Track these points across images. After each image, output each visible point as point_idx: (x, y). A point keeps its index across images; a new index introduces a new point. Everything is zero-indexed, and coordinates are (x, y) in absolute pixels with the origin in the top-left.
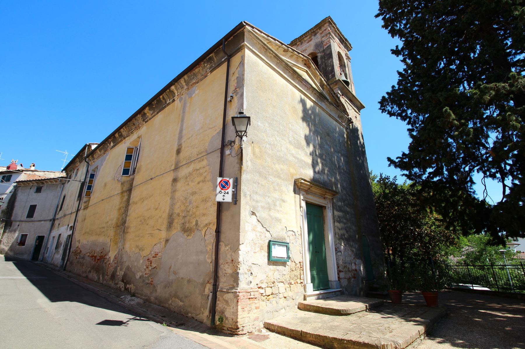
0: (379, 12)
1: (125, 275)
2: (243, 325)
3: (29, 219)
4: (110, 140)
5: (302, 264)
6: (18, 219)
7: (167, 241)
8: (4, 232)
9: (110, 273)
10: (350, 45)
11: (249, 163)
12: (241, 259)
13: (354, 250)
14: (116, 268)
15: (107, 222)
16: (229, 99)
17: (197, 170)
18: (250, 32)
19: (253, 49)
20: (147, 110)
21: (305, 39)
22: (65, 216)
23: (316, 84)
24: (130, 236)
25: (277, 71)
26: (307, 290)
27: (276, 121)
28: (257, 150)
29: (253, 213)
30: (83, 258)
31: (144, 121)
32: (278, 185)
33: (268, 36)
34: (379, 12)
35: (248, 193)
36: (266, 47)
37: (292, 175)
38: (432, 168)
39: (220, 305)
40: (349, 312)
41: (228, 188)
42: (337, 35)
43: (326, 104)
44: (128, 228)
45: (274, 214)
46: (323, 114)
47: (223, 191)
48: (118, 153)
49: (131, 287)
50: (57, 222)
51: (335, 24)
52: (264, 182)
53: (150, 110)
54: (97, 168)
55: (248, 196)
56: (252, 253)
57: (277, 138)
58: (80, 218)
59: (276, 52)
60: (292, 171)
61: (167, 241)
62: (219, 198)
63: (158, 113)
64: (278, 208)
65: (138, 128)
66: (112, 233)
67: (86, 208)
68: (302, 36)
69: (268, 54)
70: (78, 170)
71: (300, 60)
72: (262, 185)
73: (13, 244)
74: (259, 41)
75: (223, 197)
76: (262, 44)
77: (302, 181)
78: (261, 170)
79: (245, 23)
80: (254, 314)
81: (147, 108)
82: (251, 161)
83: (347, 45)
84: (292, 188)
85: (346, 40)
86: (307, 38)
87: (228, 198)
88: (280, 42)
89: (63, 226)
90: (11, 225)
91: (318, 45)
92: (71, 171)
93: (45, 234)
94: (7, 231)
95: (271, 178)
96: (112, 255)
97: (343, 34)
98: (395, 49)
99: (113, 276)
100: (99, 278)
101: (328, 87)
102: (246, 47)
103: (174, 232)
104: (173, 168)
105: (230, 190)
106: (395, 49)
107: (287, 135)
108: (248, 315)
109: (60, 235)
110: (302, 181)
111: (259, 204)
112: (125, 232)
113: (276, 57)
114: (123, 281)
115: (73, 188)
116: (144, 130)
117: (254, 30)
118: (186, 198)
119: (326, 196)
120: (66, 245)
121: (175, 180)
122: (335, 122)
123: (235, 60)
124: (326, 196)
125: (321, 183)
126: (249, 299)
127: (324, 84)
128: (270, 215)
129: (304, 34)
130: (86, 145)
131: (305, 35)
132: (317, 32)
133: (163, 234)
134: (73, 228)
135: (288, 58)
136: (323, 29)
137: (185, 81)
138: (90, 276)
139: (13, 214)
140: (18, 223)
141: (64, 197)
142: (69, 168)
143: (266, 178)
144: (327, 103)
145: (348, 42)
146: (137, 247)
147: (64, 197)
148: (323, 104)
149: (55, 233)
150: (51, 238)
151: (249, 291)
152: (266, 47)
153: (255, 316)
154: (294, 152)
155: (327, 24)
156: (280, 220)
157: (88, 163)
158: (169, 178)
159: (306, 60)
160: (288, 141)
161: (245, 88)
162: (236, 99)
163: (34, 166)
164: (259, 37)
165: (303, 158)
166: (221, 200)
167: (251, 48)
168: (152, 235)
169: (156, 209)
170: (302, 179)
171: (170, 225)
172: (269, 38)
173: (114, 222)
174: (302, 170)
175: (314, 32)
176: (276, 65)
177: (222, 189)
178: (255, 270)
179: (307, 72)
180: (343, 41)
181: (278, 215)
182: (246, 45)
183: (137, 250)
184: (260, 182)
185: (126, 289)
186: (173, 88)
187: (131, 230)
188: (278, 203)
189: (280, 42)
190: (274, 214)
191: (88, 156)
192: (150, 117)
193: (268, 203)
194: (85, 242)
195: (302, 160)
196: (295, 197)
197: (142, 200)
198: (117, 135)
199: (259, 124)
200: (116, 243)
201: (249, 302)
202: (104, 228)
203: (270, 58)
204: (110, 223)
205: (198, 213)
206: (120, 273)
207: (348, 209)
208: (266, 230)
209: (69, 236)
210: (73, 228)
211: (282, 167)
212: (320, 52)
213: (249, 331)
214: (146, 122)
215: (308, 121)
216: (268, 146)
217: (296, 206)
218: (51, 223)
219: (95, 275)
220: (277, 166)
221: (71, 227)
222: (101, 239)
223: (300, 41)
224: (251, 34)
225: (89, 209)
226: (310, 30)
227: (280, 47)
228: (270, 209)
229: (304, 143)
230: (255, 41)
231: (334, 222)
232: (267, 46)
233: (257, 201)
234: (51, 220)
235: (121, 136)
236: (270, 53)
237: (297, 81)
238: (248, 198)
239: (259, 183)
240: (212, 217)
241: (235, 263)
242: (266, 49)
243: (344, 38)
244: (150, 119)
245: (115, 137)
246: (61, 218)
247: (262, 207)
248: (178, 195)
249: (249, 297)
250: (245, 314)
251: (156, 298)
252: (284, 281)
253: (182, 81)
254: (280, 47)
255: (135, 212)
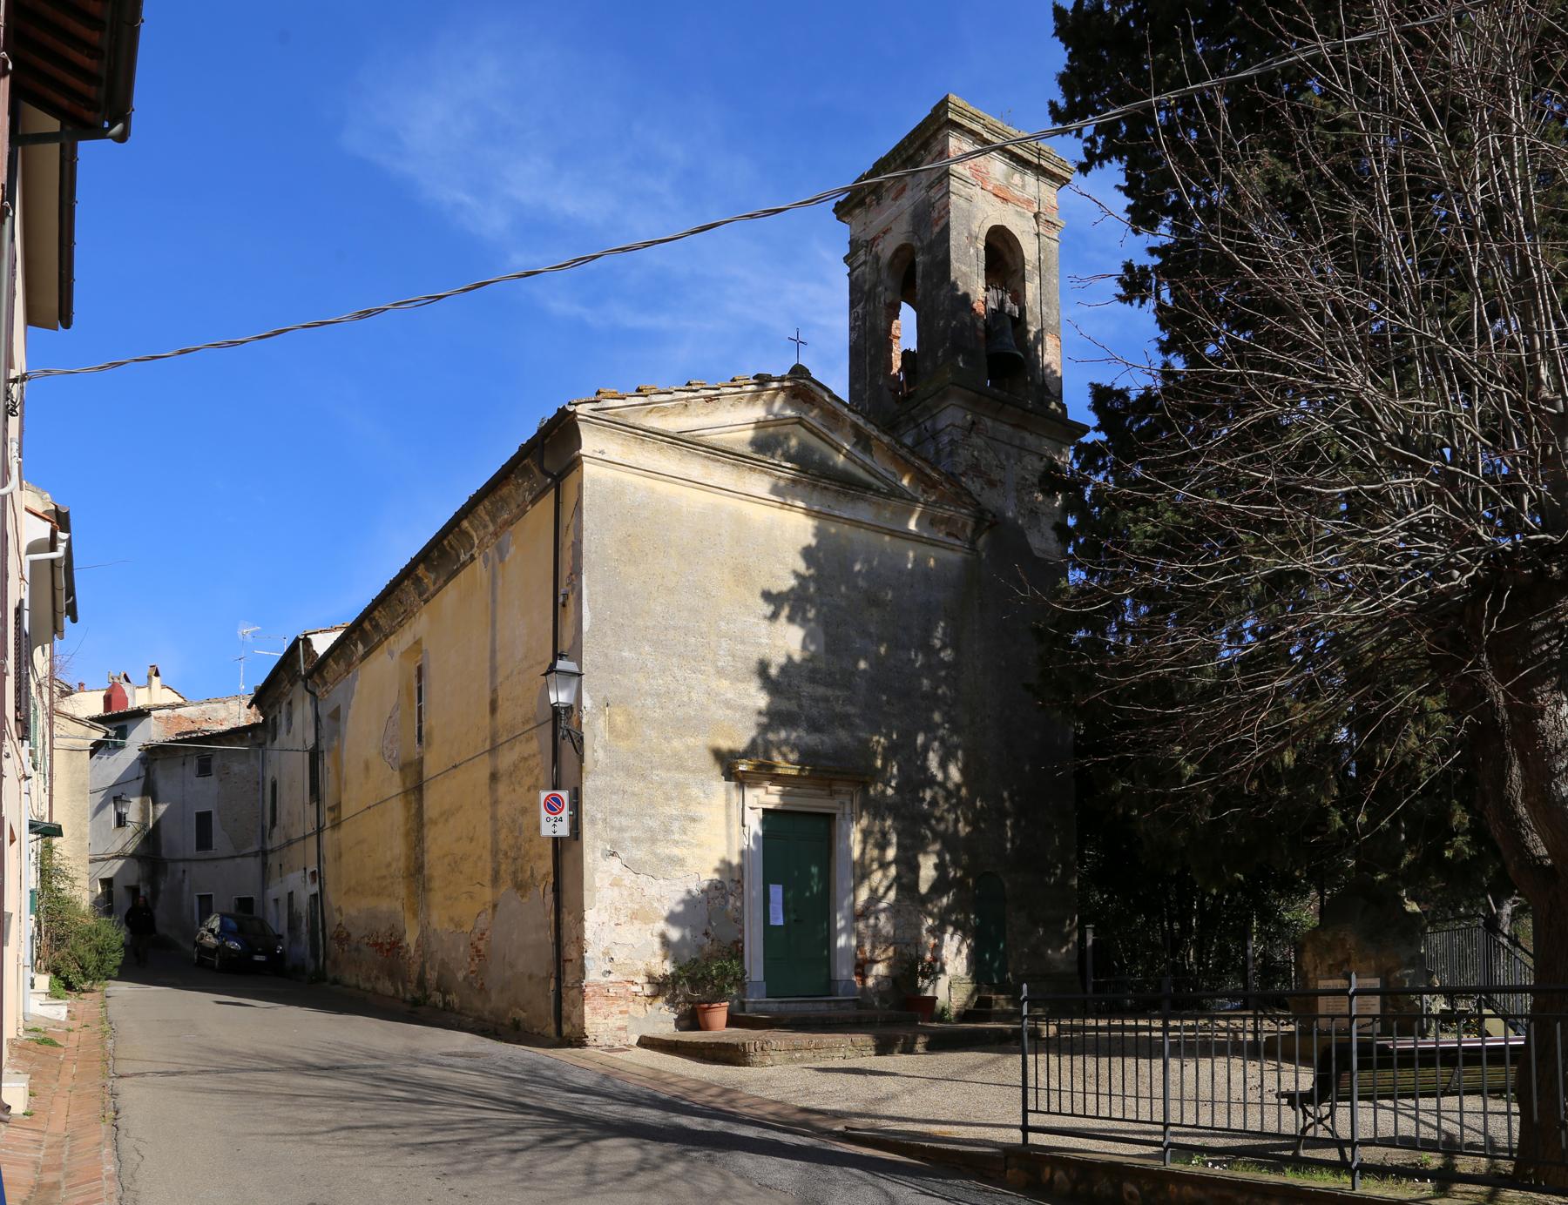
1: (440, 977)
3: (203, 854)
4: (355, 636)
6: (179, 856)
7: (495, 906)
9: (414, 976)
11: (600, 755)
12: (588, 935)
14: (423, 965)
15: (389, 865)
16: (561, 599)
17: (525, 759)
20: (421, 570)
22: (290, 843)
24: (437, 897)
27: (675, 628)
28: (619, 720)
30: (357, 949)
31: (420, 595)
35: (599, 816)
38: (926, 748)
39: (566, 1007)
44: (431, 879)
45: (664, 849)
48: (381, 672)
49: (453, 998)
50: (273, 860)
52: (638, 787)
53: (427, 569)
54: (337, 710)
57: (678, 674)
58: (328, 853)
61: (495, 906)
62: (547, 830)
63: (446, 583)
64: (676, 837)
65: (409, 614)
66: (401, 890)
67: (336, 824)
70: (290, 703)
72: (634, 794)
78: (631, 761)
80: (616, 1021)
81: (422, 566)
82: (604, 748)
87: (563, 830)
89: (291, 870)
92: (272, 706)
93: (250, 892)
95: (659, 775)
96: (411, 938)
99: (421, 983)
100: (397, 991)
103: (503, 890)
104: (487, 747)
105: (565, 814)
107: (710, 657)
109: (291, 894)
111: (627, 835)
112: (426, 889)
114: (438, 989)
115: (289, 765)
116: (420, 625)
118: (514, 821)
120: (313, 921)
121: (494, 777)
123: (569, 484)
128: (654, 854)
130: (297, 640)
133: (488, 894)
134: (317, 876)
137: (488, 513)
138: (380, 986)
140: (181, 866)
141: (274, 786)
142: (264, 697)
143: (643, 777)
146: (451, 919)
147: (274, 786)
148: (862, 505)
149: (276, 890)
150: (271, 905)
153: (619, 1023)
156: (682, 860)
157: (313, 693)
158: (482, 772)
160: (712, 671)
161: (584, 578)
162: (572, 598)
163: (157, 674)
168: (471, 895)
169: (472, 840)
171: (496, 879)
173: (402, 864)
181: (677, 851)
183: (452, 928)
185: (446, 1004)
186: (465, 524)
187: (436, 884)
188: (676, 826)
190: (664, 849)
191: (310, 675)
192: (432, 588)
193: (651, 830)
194: (353, 912)
197: (447, 815)
198: (367, 625)
199: (626, 654)
200: (415, 915)
202: (384, 877)
204: (394, 865)
205: (532, 853)
206: (432, 976)
209: (315, 896)
210: (317, 876)
214: (426, 601)
216: (649, 701)
218: (259, 860)
219: (388, 984)
220: (676, 743)
221: (313, 873)
222: (384, 905)
225: (345, 829)
228: (654, 841)
233: (621, 830)
234: (256, 854)
235: (376, 627)
238: (600, 825)
239: (624, 792)
240: (547, 865)
241: (580, 940)
244: (433, 595)
245: (363, 630)
246: (281, 848)
247: (635, 840)
248: (502, 810)
250: (599, 1019)
251: (491, 1013)
253: (481, 510)
255: (439, 841)
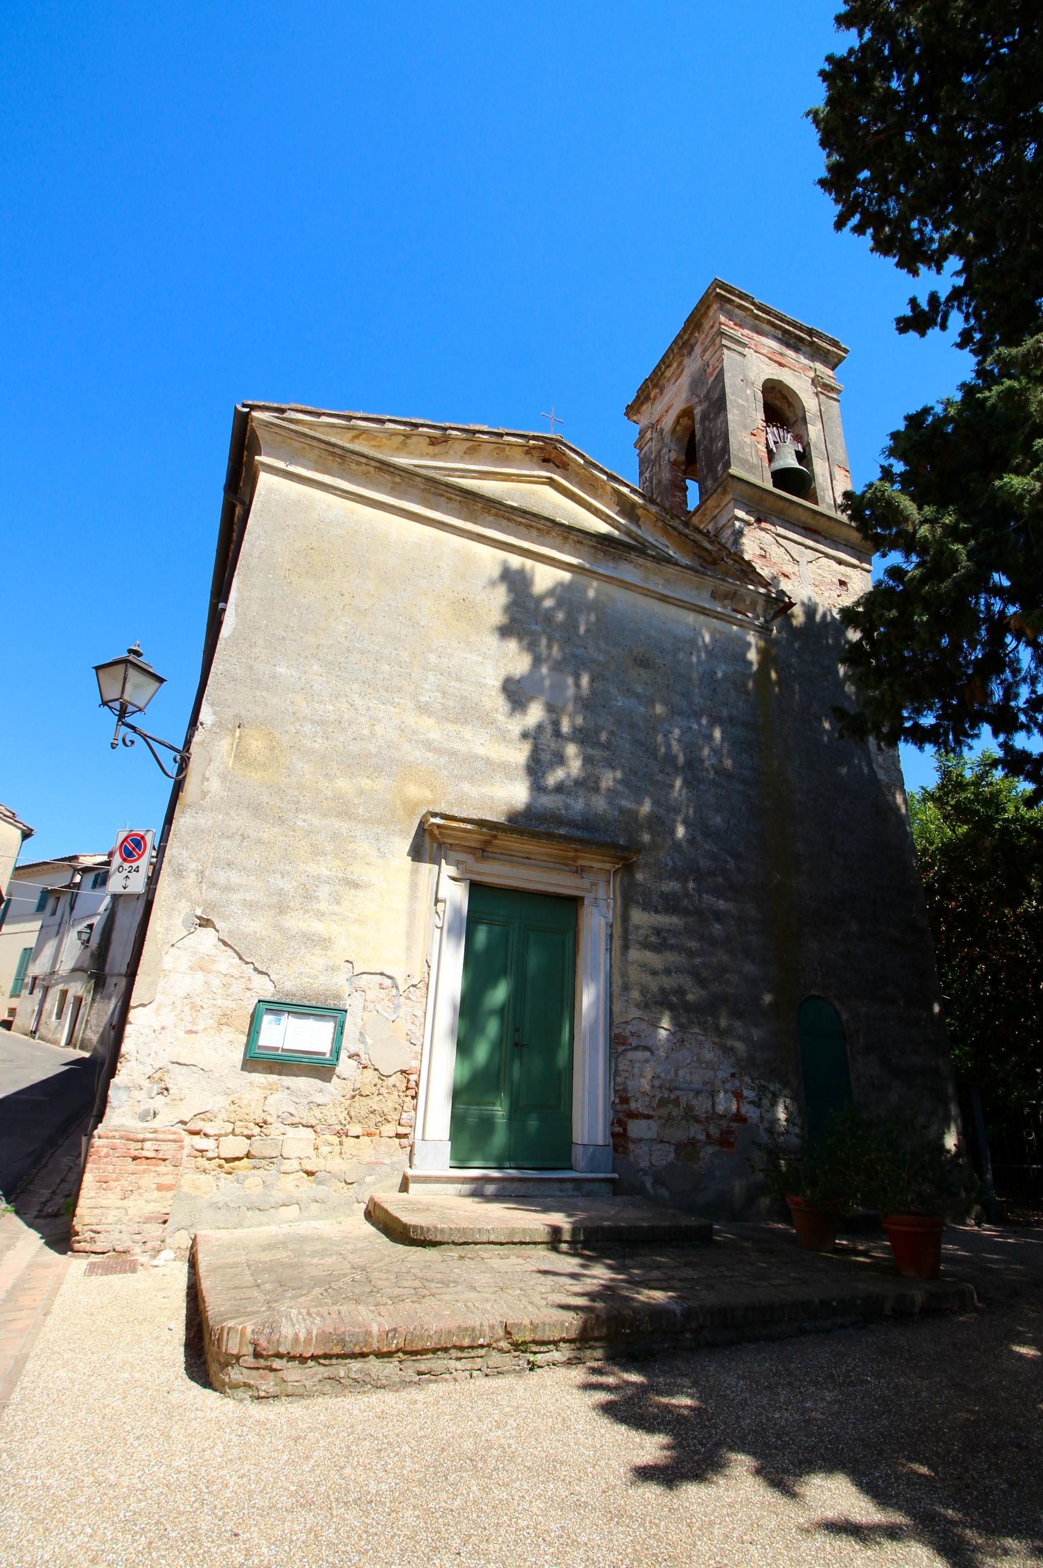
0: (839, 208)
2: (98, 1228)
5: (413, 1078)
8: (93, 1000)
10: (835, 344)
11: (215, 785)
13: (740, 1046)
18: (268, 424)
19: (292, 468)
21: (668, 374)
23: (596, 512)
25: (392, 506)
26: (416, 1160)
29: (205, 923)
32: (335, 837)
33: (350, 418)
34: (839, 208)
36: (339, 451)
37: (410, 807)
40: (431, 1237)
41: (140, 856)
42: (767, 328)
43: (637, 566)
45: (295, 922)
46: (623, 598)
47: (126, 865)
51: (742, 296)
55: (193, 876)
56: (181, 1034)
57: (359, 702)
59: (380, 456)
60: (413, 791)
68: (658, 367)
69: (353, 466)
71: (518, 453)
73: (105, 1028)
74: (309, 441)
75: (129, 882)
76: (323, 446)
77: (437, 821)
79: (244, 406)
82: (223, 777)
83: (819, 348)
84: (405, 844)
85: (810, 332)
86: (672, 369)
88: (405, 424)
90: (103, 986)
91: (696, 383)
94: (98, 997)
97: (790, 316)
98: (907, 312)
101: (654, 509)
102: (260, 467)
105: (144, 863)
106: (907, 312)
108: (119, 1203)
110: (437, 821)
111: (235, 897)
113: (385, 467)
117: (289, 415)
119: (580, 862)
122: (690, 618)
124: (580, 862)
125: (570, 823)
126: (135, 1158)
127: (634, 505)
128: (279, 928)
129: (663, 360)
131: (665, 362)
132: (692, 341)
135: (462, 460)
136: (706, 326)
139: (109, 960)
143: (281, 820)
144: (640, 561)
145: (820, 336)
151: (140, 1136)
152: (339, 451)
154: (435, 735)
155: (715, 306)
159: (541, 448)
164: (307, 431)
165: (481, 751)
166: (119, 890)
167: (281, 465)
170: (435, 815)
172: (354, 422)
174: (466, 787)
175: (685, 344)
176: (393, 491)
177: (125, 860)
178: (178, 1080)
179: (551, 483)
180: (801, 340)
181: (318, 927)
182: (263, 464)
184: (250, 832)
189: (405, 424)
193: (280, 892)
195: (476, 757)
196: (415, 872)
199: (281, 670)
201: (132, 1166)
203: (365, 480)
207: (722, 904)
208: (256, 969)
211: (366, 783)
212: (700, 402)
213: (119, 1248)
215: (532, 633)
216: (308, 728)
217: (413, 897)
220: (343, 784)
223: (655, 386)
224: (277, 430)
226: (675, 342)
227: (407, 436)
229: (501, 703)
230: (298, 445)
231: (626, 947)
232: (342, 448)
233: (227, 888)
236: (359, 463)
237: (491, 518)
242: (341, 457)
243: (801, 328)
249: (136, 1153)
250: (111, 1199)
252: (314, 1122)
254: (407, 436)
